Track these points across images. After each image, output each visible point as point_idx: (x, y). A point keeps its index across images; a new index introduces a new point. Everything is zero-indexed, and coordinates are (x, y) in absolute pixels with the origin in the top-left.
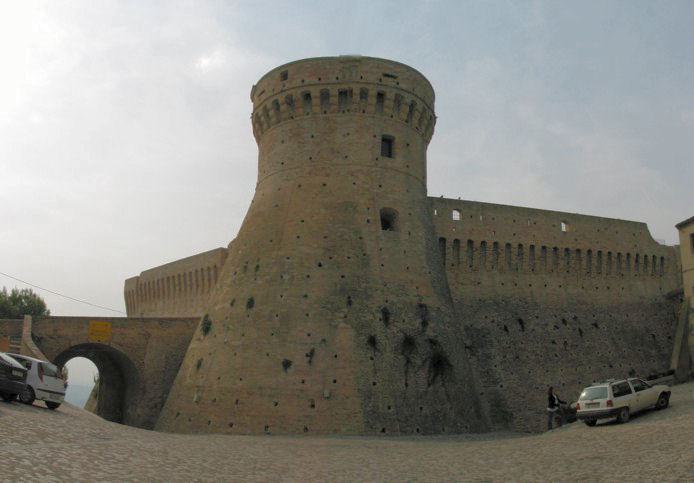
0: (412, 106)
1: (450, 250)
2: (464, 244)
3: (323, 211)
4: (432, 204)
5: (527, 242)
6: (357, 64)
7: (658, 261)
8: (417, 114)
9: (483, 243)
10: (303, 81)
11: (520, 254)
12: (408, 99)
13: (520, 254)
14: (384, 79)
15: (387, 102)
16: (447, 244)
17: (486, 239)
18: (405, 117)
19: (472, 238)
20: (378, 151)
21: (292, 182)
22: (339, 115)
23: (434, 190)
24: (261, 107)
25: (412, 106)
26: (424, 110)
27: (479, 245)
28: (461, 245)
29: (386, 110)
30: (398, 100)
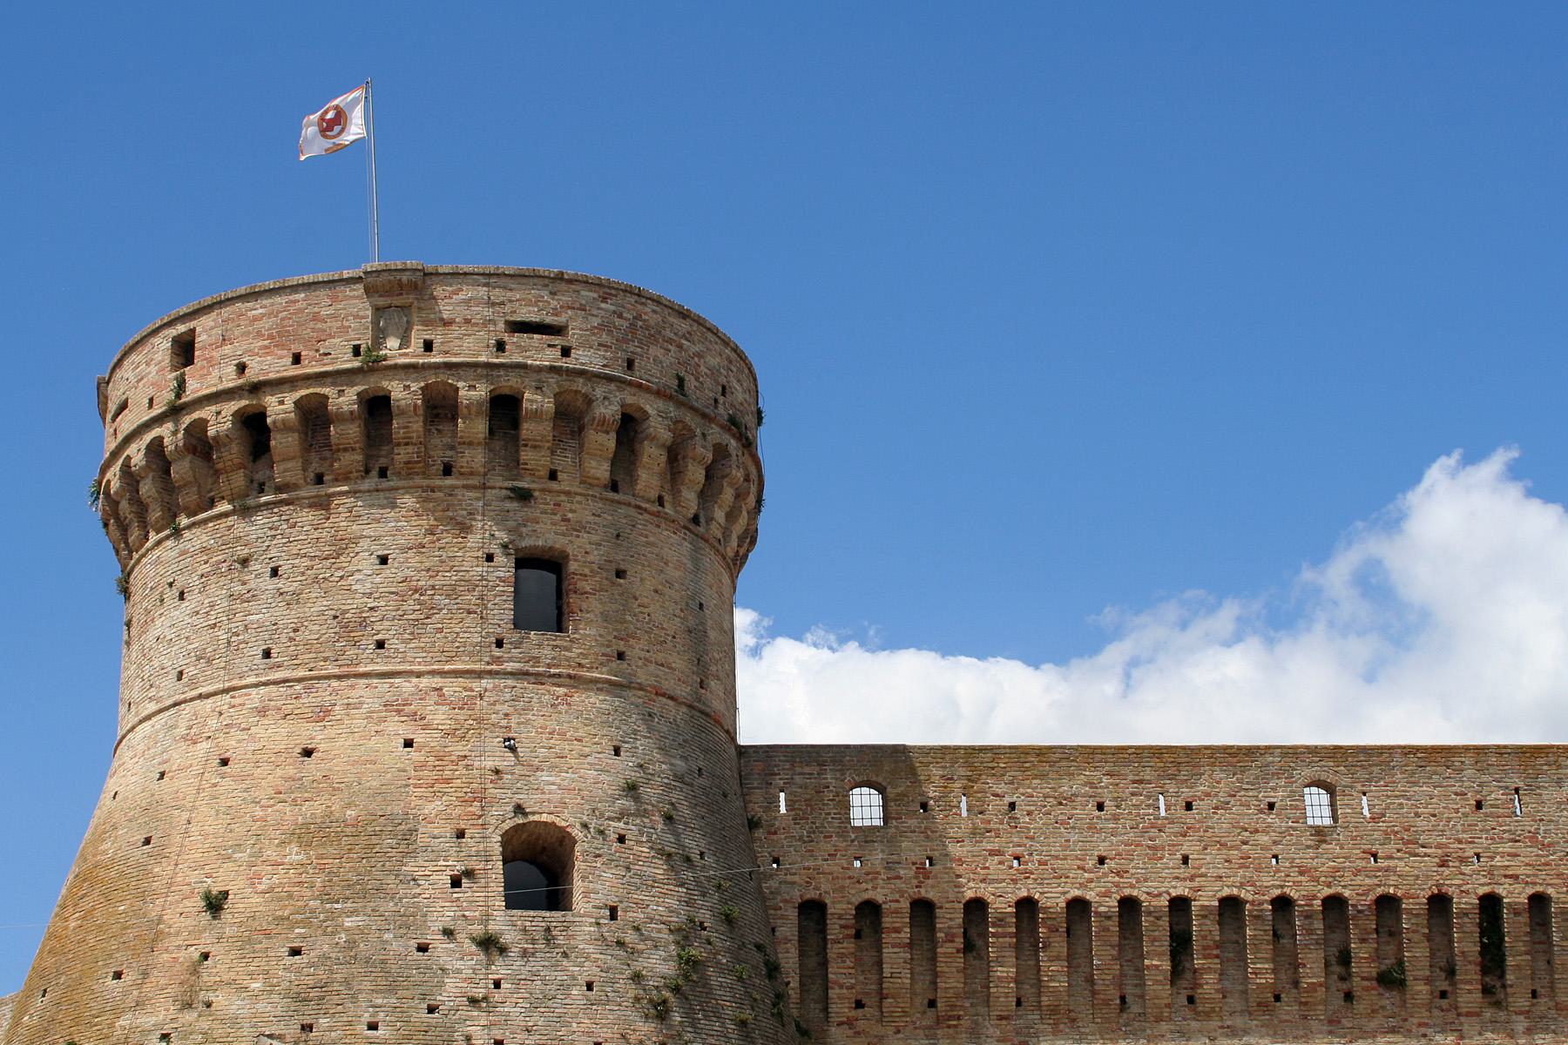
0: (629, 427)
1: (840, 947)
2: (897, 922)
3: (294, 854)
4: (768, 776)
5: (1155, 889)
6: (410, 298)
7: (1514, 928)
8: (652, 458)
9: (1129, 906)
10: (242, 368)
11: (1180, 944)
12: (608, 408)
13: (1180, 944)
14: (512, 340)
15: (528, 429)
16: (834, 930)
17: (986, 892)
18: (601, 470)
19: (930, 894)
20: (502, 612)
21: (204, 745)
22: (367, 484)
23: (748, 734)
24: (116, 468)
25: (629, 427)
26: (721, 452)
27: (959, 918)
28: (887, 921)
29: (526, 455)
30: (440, 408)
